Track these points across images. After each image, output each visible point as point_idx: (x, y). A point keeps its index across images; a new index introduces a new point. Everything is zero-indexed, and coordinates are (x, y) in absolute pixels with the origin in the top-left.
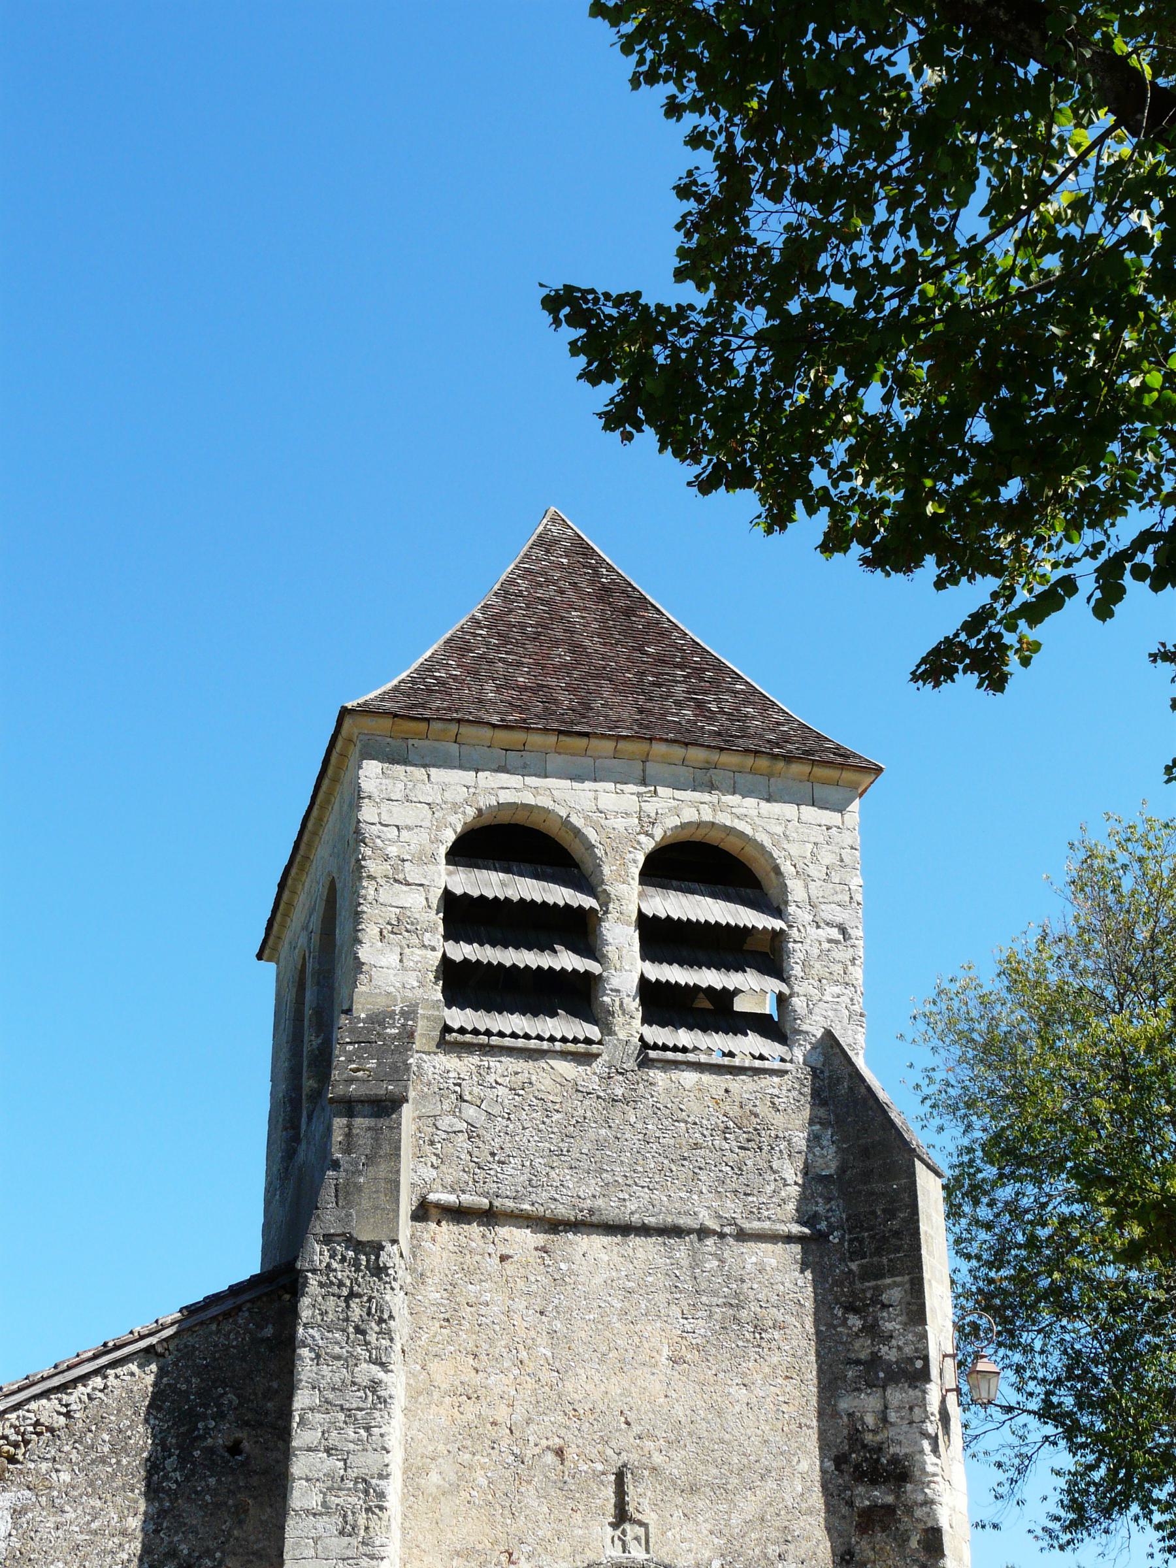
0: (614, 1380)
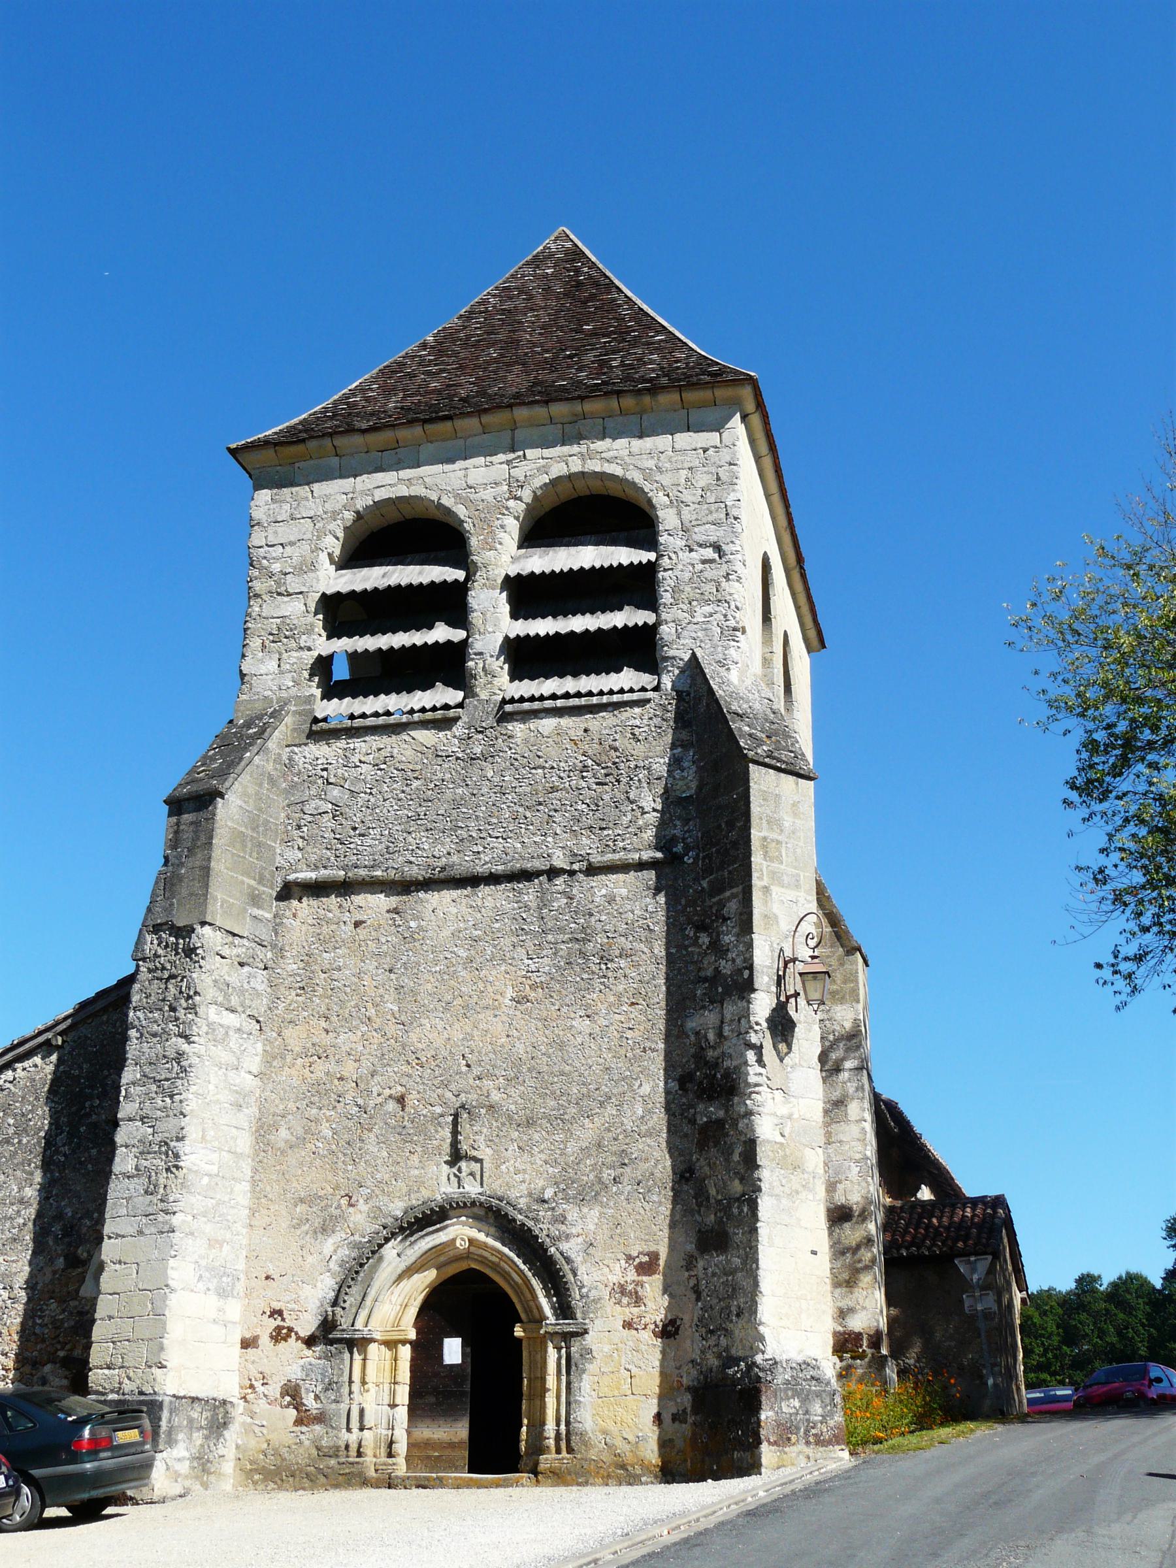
0: (457, 1026)
